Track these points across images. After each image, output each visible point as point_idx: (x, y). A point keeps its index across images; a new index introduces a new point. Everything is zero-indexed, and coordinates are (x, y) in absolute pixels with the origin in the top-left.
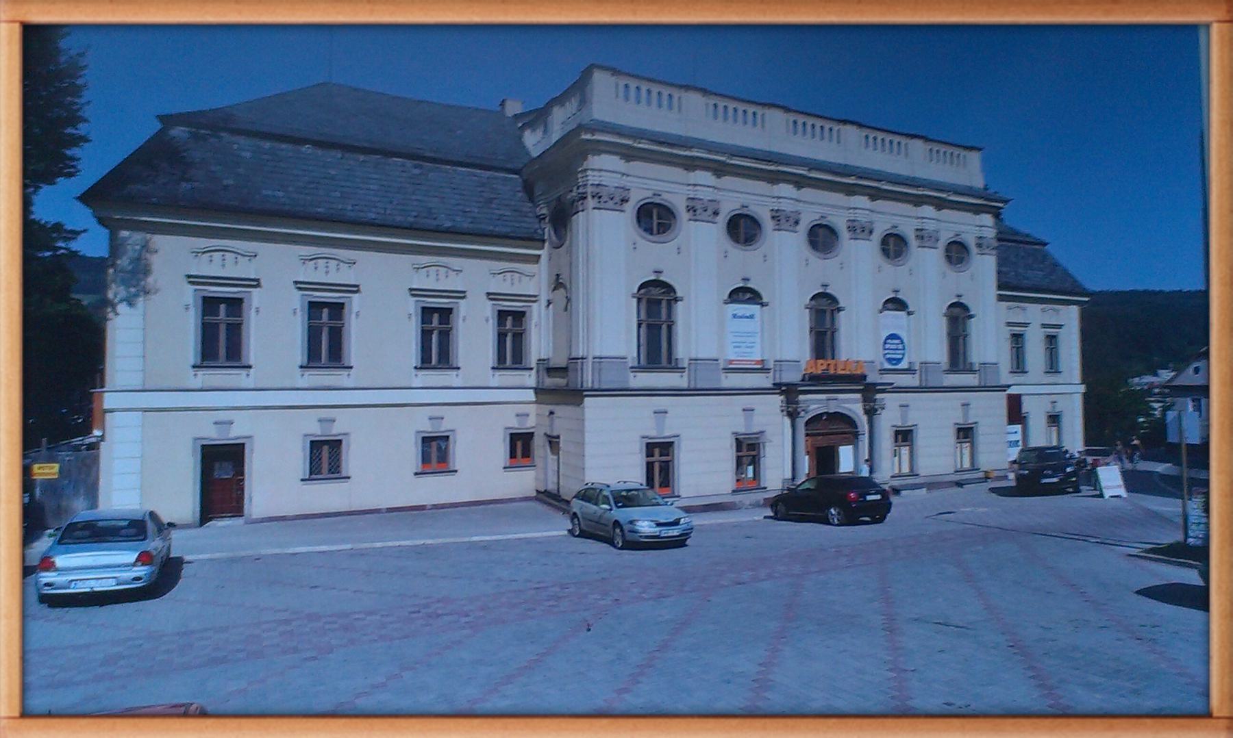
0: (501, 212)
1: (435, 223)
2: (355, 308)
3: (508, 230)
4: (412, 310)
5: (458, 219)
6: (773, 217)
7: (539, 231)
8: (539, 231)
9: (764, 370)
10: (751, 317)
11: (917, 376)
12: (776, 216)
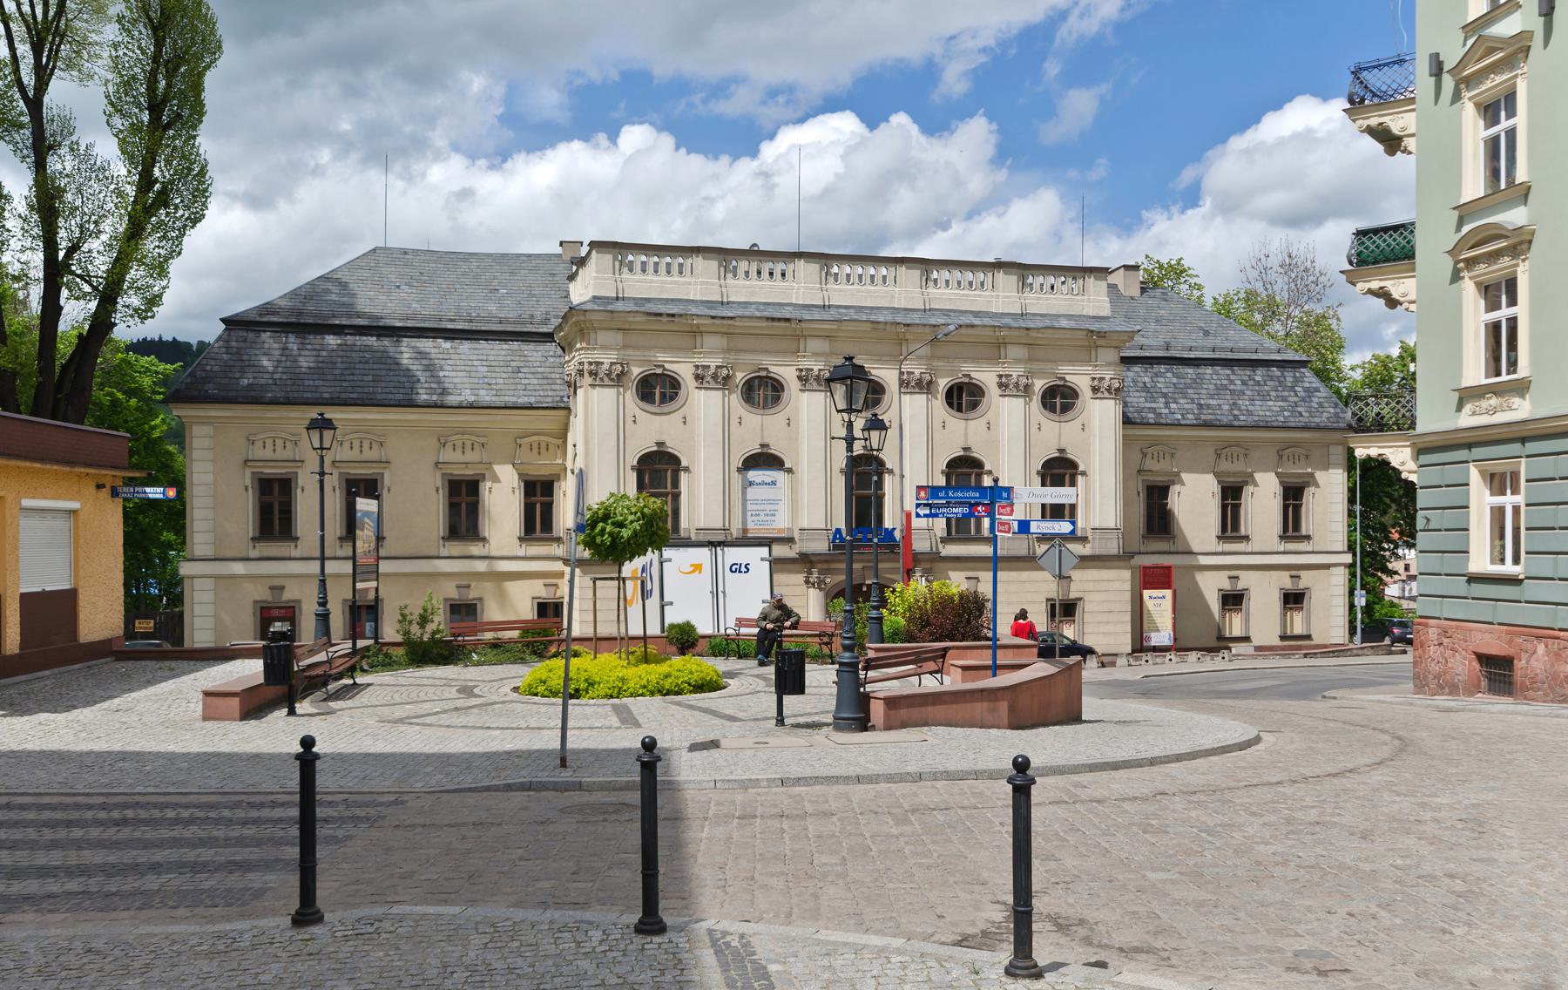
0: (527, 381)
1: (459, 398)
2: (387, 482)
3: (532, 400)
4: (439, 484)
5: (482, 392)
6: (799, 378)
7: (565, 399)
8: (565, 399)
9: (789, 540)
10: (774, 483)
11: (1088, 546)
12: (804, 378)
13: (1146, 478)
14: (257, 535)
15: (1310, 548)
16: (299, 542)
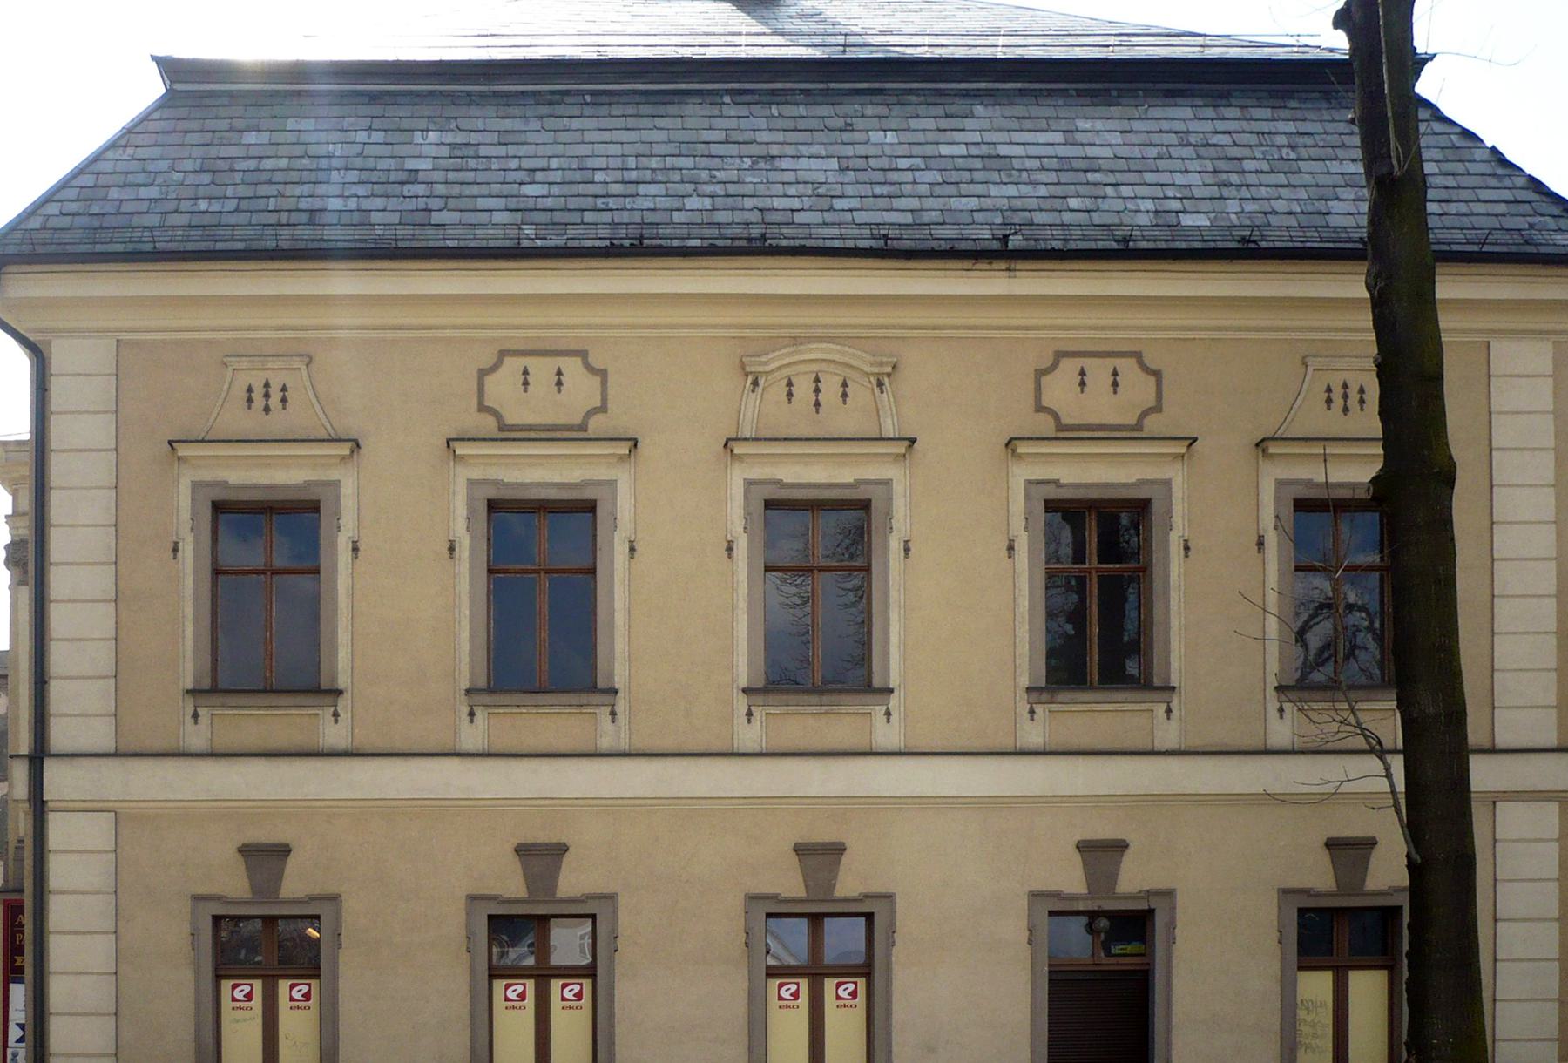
13: (1040, 472)
14: (482, 682)
15: (1169, 735)
16: (343, 703)
